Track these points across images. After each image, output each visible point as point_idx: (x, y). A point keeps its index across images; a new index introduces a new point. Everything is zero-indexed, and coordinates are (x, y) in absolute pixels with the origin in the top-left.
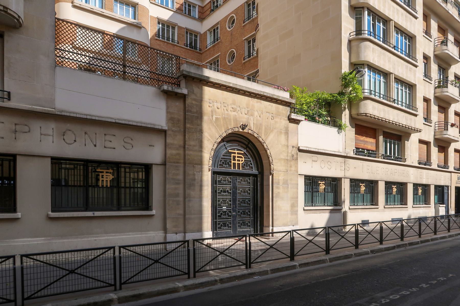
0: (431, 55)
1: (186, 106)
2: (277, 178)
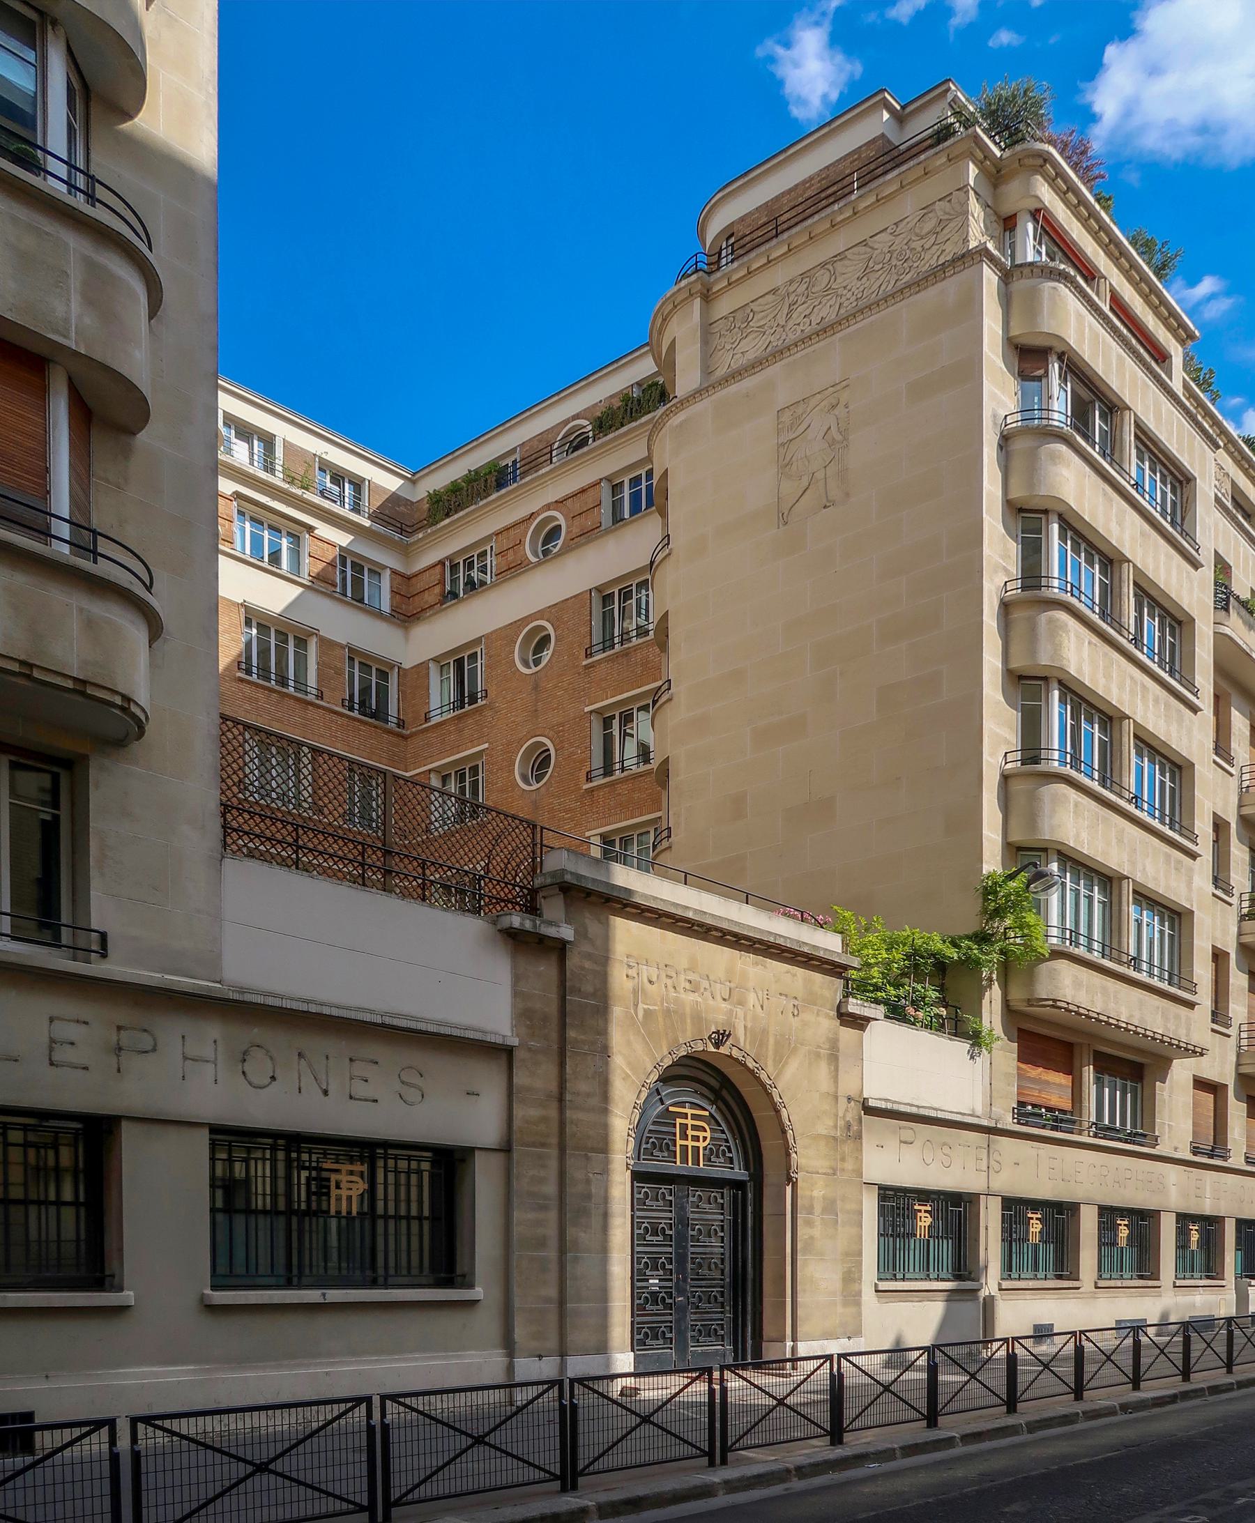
2: (808, 1193)
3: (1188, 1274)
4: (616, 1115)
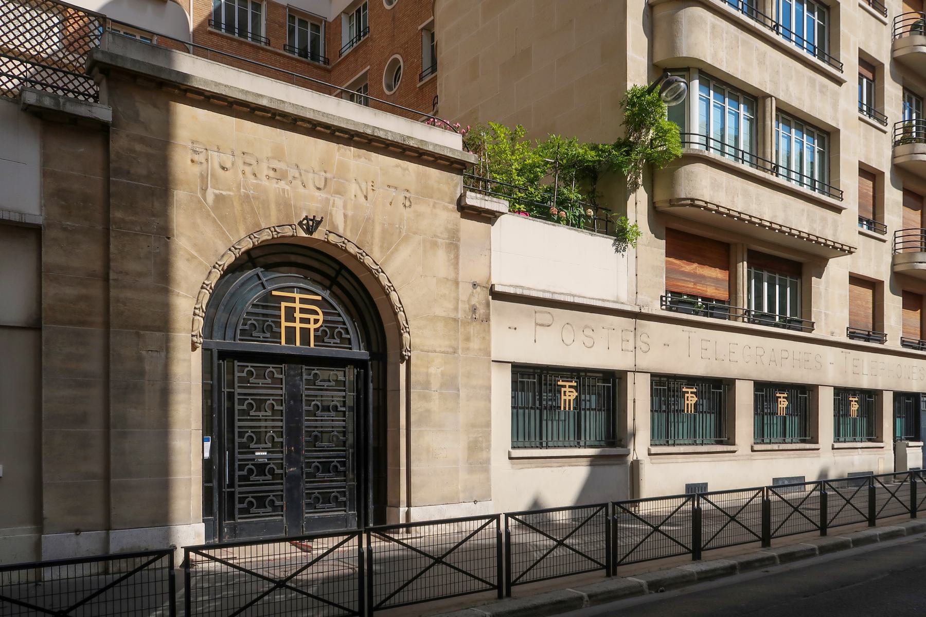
0: (885, 58)
1: (112, 156)
2: (423, 370)
3: (663, 441)
4: (178, 295)
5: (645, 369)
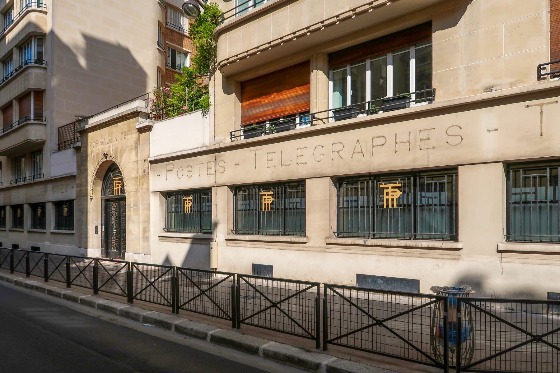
3: (545, 236)
5: (490, 156)
